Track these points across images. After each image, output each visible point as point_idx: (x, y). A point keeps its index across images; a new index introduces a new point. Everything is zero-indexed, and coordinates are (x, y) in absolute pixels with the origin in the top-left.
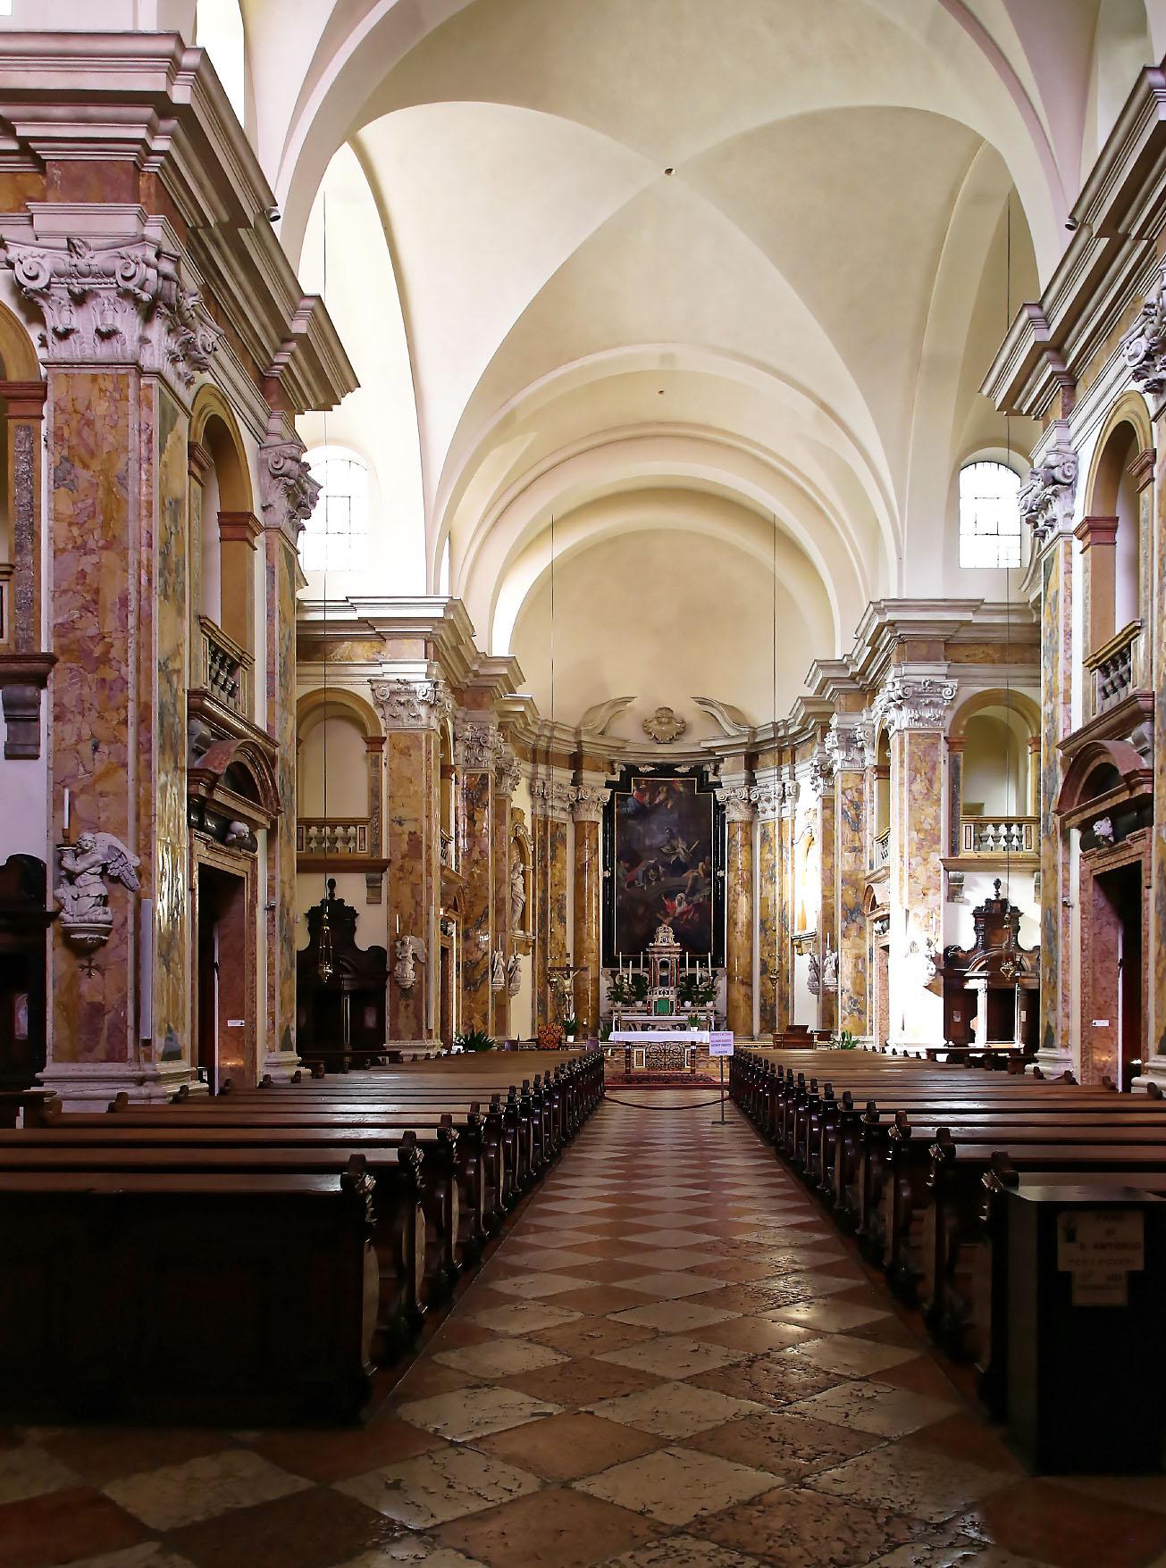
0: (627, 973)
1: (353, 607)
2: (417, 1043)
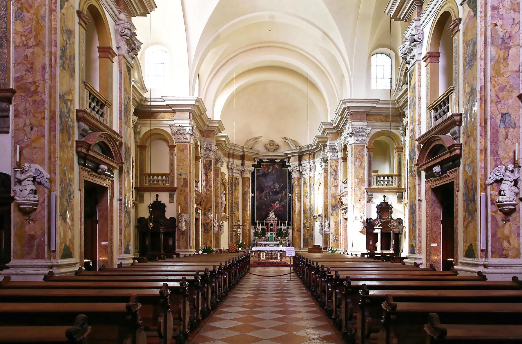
0: (260, 227)
1: (164, 100)
2: (186, 250)
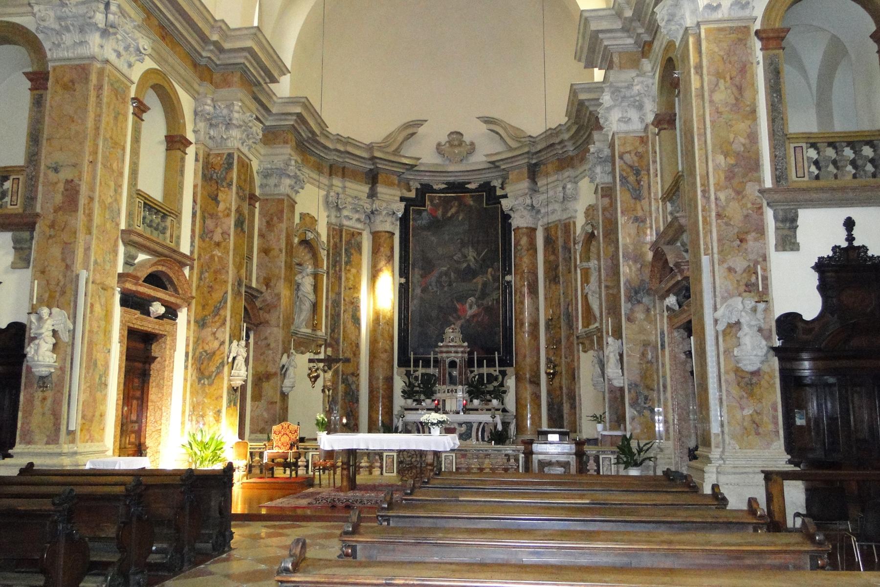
2: (52, 448)
